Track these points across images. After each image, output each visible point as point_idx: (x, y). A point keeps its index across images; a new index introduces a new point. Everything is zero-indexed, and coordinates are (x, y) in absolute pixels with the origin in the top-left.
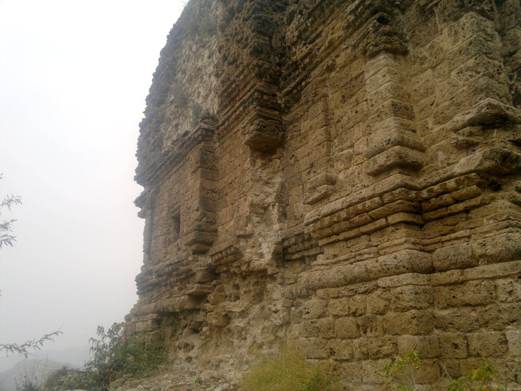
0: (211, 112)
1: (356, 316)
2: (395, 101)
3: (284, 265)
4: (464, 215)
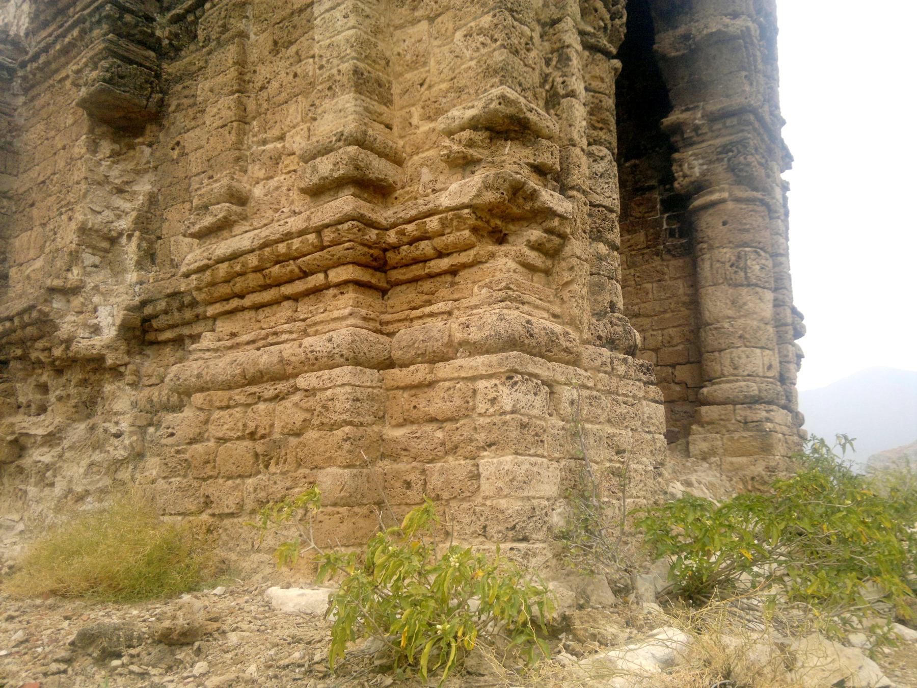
0: (13, 31)
1: (255, 439)
2: (361, 65)
3: (143, 350)
4: (449, 278)
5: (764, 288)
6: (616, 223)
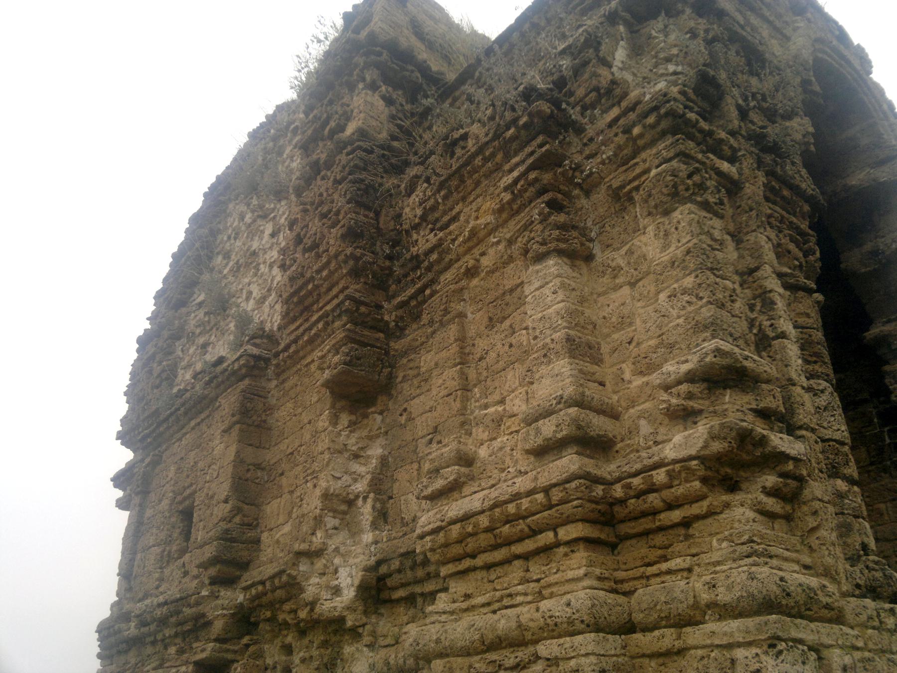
3: (377, 609)
4: (682, 531)
6: (850, 456)
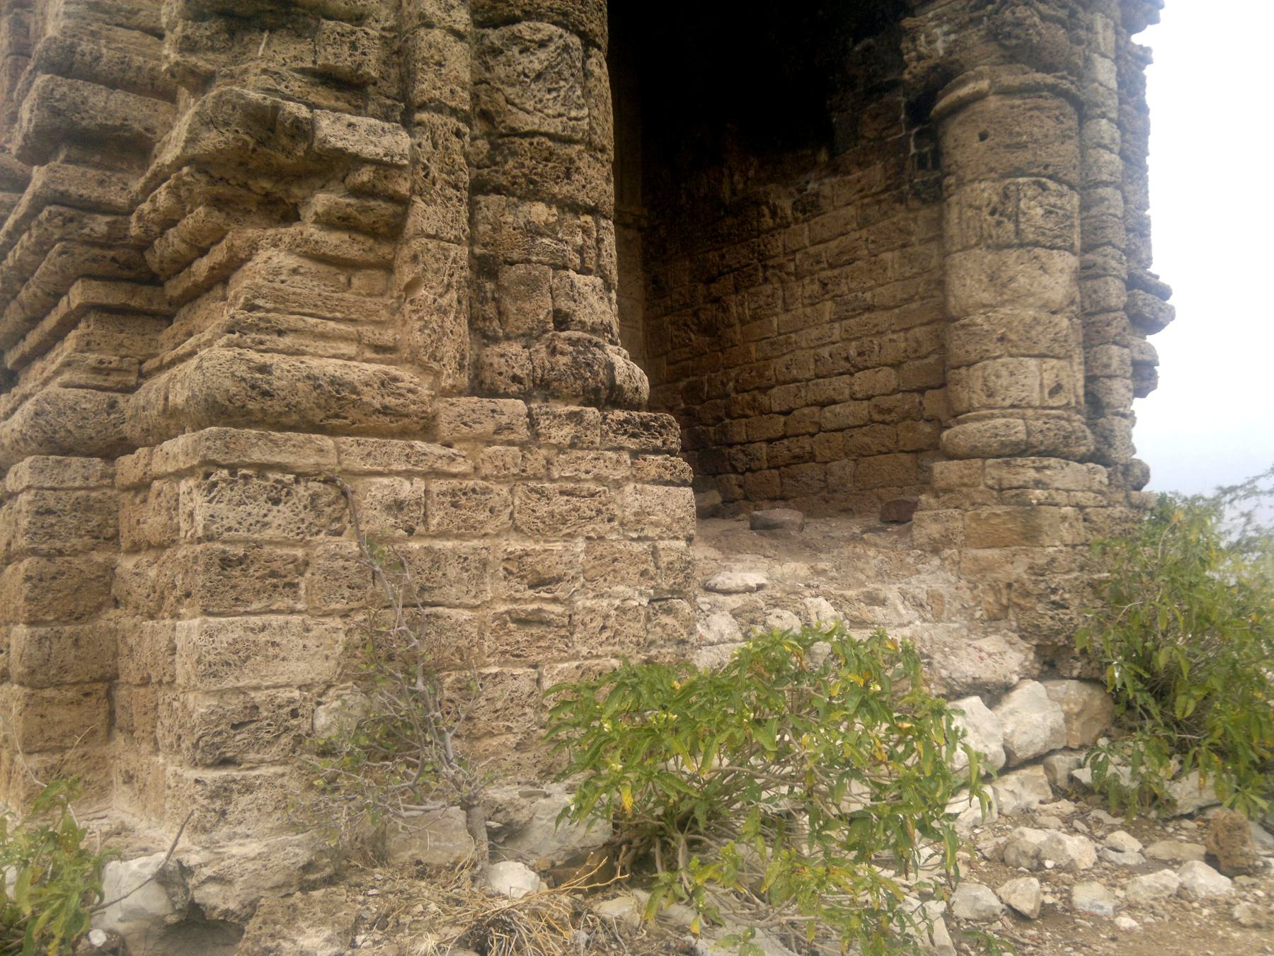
5: (1052, 248)
